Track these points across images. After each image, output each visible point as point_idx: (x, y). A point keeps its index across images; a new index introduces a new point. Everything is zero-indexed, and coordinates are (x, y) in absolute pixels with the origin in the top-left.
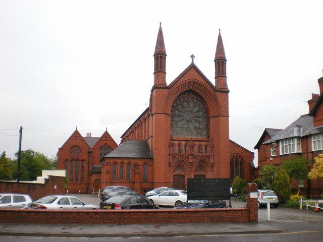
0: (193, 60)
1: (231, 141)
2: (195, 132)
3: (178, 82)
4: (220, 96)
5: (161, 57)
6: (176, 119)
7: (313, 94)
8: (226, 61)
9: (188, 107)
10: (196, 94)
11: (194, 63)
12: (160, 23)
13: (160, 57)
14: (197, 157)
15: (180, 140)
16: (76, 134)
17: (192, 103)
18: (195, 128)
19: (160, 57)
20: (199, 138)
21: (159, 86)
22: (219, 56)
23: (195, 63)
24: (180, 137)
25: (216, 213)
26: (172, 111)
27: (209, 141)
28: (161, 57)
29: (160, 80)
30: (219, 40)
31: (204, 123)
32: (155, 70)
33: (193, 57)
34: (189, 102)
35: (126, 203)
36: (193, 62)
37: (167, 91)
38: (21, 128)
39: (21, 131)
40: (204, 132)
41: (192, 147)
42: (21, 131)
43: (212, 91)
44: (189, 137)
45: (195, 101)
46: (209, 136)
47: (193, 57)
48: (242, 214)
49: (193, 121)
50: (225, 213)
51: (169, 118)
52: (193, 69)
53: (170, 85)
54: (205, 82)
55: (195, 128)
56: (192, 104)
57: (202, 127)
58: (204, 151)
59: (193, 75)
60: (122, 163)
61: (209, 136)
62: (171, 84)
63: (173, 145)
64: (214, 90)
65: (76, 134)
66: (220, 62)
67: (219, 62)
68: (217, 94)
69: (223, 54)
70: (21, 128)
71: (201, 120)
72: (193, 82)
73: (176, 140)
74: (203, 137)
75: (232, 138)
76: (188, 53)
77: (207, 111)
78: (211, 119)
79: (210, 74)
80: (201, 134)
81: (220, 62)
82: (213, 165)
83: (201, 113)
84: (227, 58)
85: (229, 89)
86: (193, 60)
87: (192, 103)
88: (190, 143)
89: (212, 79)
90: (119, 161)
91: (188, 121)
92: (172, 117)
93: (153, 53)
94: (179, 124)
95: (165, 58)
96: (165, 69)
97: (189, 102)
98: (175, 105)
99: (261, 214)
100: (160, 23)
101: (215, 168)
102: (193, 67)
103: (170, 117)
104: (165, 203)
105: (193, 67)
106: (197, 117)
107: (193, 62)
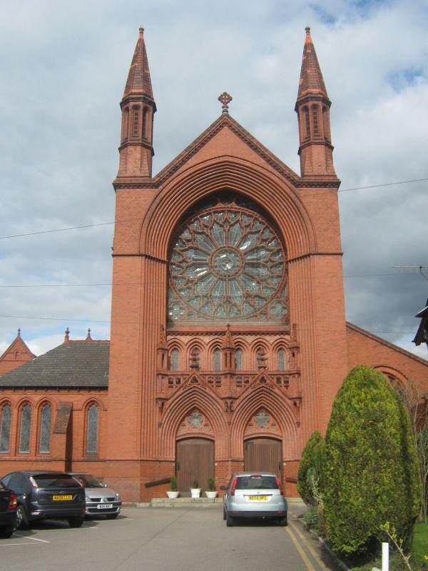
2: (247, 309)
9: (227, 238)
10: (226, 195)
13: (139, 105)
15: (197, 333)
19: (139, 105)
22: (303, 93)
23: (232, 113)
24: (199, 324)
28: (145, 110)
33: (225, 99)
37: (149, 194)
39: (339, 254)
41: (233, 350)
42: (339, 254)
43: (285, 186)
44: (221, 325)
45: (246, 220)
47: (225, 99)
53: (158, 176)
54: (262, 162)
55: (247, 296)
57: (268, 293)
59: (225, 145)
60: (25, 403)
64: (293, 182)
66: (313, 106)
67: (306, 109)
68: (302, 191)
70: (342, 254)
71: (263, 272)
72: (224, 167)
73: (183, 334)
74: (270, 323)
76: (228, 80)
78: (174, 460)
79: (281, 139)
81: (313, 106)
82: (297, 402)
86: (225, 108)
87: (237, 226)
92: (168, 264)
94: (201, 288)
101: (306, 411)
105: (225, 122)
106: (253, 265)
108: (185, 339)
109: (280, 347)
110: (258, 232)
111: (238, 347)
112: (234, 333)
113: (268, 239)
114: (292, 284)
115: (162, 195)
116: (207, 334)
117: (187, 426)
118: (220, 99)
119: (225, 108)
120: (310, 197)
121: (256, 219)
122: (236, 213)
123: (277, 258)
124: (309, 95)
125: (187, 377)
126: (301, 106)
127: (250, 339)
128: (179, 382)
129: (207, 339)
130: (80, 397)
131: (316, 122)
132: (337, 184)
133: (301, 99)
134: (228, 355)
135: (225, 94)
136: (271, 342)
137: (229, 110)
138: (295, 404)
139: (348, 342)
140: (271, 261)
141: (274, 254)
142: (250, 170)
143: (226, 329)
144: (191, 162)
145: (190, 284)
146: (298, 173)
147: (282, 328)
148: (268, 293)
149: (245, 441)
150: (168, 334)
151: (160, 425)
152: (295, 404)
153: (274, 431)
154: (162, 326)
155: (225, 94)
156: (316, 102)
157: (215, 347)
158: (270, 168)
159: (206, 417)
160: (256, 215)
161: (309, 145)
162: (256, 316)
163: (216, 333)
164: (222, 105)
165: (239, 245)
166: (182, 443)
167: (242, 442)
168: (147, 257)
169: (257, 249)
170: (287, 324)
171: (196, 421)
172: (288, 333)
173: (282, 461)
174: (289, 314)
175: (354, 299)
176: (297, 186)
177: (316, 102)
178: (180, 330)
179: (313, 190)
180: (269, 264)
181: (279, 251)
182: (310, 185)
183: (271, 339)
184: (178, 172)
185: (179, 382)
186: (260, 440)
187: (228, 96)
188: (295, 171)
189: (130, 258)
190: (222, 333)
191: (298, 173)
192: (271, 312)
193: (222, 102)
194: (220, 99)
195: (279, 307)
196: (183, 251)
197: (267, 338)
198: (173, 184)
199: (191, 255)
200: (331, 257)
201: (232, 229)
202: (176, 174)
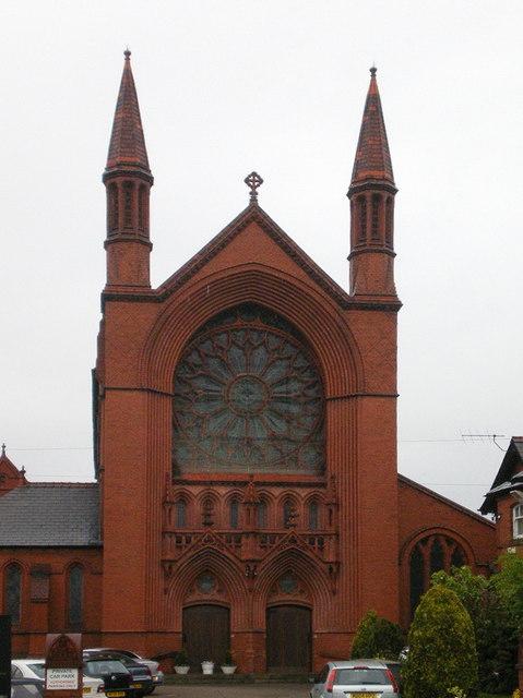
2: (271, 454)
3: (197, 277)
13: (128, 184)
15: (211, 483)
18: (273, 437)
19: (128, 184)
21: (124, 292)
23: (263, 204)
24: (211, 470)
33: (254, 181)
36: (254, 200)
37: (149, 312)
45: (274, 342)
47: (254, 181)
55: (273, 437)
66: (372, 197)
68: (352, 315)
71: (295, 409)
72: (254, 277)
74: (302, 472)
79: (324, 238)
81: (372, 197)
82: (334, 570)
86: (254, 194)
87: (261, 350)
93: (100, 164)
94: (213, 426)
107: (254, 200)
108: (195, 490)
109: (313, 502)
110: (289, 358)
111: (264, 501)
112: (257, 484)
113: (302, 367)
114: (331, 427)
116: (223, 483)
117: (197, 592)
118: (247, 181)
119: (254, 194)
120: (360, 324)
121: (287, 341)
123: (311, 393)
125: (200, 536)
127: (277, 491)
128: (188, 541)
129: (223, 491)
131: (375, 220)
133: (358, 184)
134: (252, 511)
135: (254, 174)
136: (303, 495)
138: (331, 569)
140: (305, 395)
141: (308, 388)
145: (201, 420)
147: (316, 480)
148: (301, 434)
149: (268, 609)
150: (175, 482)
152: (331, 569)
153: (302, 599)
154: (167, 476)
155: (254, 174)
156: (377, 192)
157: (233, 501)
158: (312, 284)
163: (234, 483)
164: (250, 190)
166: (190, 610)
167: (263, 613)
168: (149, 390)
169: (286, 380)
170: (323, 474)
171: (205, 585)
172: (323, 485)
175: (444, 440)
176: (345, 309)
178: (191, 478)
180: (302, 400)
181: (313, 385)
182: (363, 307)
183: (303, 493)
185: (188, 541)
186: (286, 609)
187: (259, 177)
188: (342, 287)
190: (245, 483)
193: (249, 185)
194: (247, 181)
195: (312, 453)
196: (191, 379)
197: (298, 490)
199: (201, 383)
201: (256, 353)
202: (188, 284)
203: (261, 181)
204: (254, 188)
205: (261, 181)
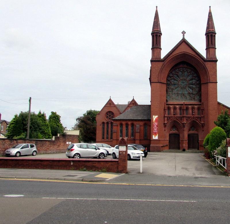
0: (184, 35)
1: (219, 104)
3: (171, 55)
4: (208, 65)
5: (212, 35)
6: (172, 87)
7: (110, 100)
8: (216, 34)
11: (185, 38)
12: (157, 7)
13: (156, 36)
14: (170, 119)
15: (175, 105)
16: (110, 103)
17: (186, 72)
18: (189, 93)
19: (156, 36)
20: (193, 102)
22: (208, 30)
23: (187, 38)
24: (176, 102)
25: (90, 163)
26: (167, 80)
27: (201, 105)
28: (212, 35)
29: (155, 54)
30: (209, 16)
31: (197, 89)
32: (152, 47)
33: (184, 33)
34: (183, 72)
35: (100, 158)
36: (184, 37)
37: (161, 63)
38: (30, 98)
40: (197, 98)
44: (182, 102)
45: (189, 70)
46: (200, 101)
47: (184, 33)
48: (112, 165)
49: (187, 88)
50: (97, 163)
51: (164, 87)
52: (184, 44)
53: (164, 58)
56: (186, 73)
57: (194, 93)
58: (172, 113)
59: (184, 49)
61: (200, 101)
62: (165, 57)
63: (169, 109)
65: (110, 103)
66: (211, 36)
68: (206, 63)
69: (213, 27)
70: (30, 98)
71: (194, 86)
72: (184, 55)
75: (219, 100)
76: (183, 28)
77: (199, 80)
79: (201, 48)
80: (194, 99)
81: (211, 36)
83: (194, 81)
84: (216, 32)
85: (217, 58)
86: (184, 35)
87: (186, 72)
88: (184, 108)
89: (203, 53)
90: (124, 123)
91: (183, 88)
92: (167, 84)
94: (175, 91)
95: (215, 36)
96: (160, 45)
97: (183, 72)
98: (171, 75)
99: (130, 165)
100: (157, 7)
102: (184, 42)
103: (165, 85)
104: (84, 155)
105: (184, 42)
107: (184, 37)
115: (165, 64)
122: (186, 68)
124: (210, 32)
126: (207, 34)
130: (142, 122)
132: (216, 61)
135: (184, 31)
137: (185, 36)
139: (218, 108)
142: (192, 57)
143: (183, 103)
144: (174, 54)
146: (205, 57)
151: (165, 130)
155: (184, 31)
159: (156, 48)
160: (185, 66)
161: (209, 48)
162: (192, 99)
165: (187, 78)
173: (198, 140)
174: (201, 99)
177: (211, 34)
178: (170, 103)
179: (209, 63)
180: (196, 84)
184: (169, 58)
189: (155, 84)
190: (182, 105)
191: (205, 57)
192: (196, 98)
198: (168, 60)
200: (214, 83)
203: (185, 33)
204: (184, 34)
205: (185, 33)
